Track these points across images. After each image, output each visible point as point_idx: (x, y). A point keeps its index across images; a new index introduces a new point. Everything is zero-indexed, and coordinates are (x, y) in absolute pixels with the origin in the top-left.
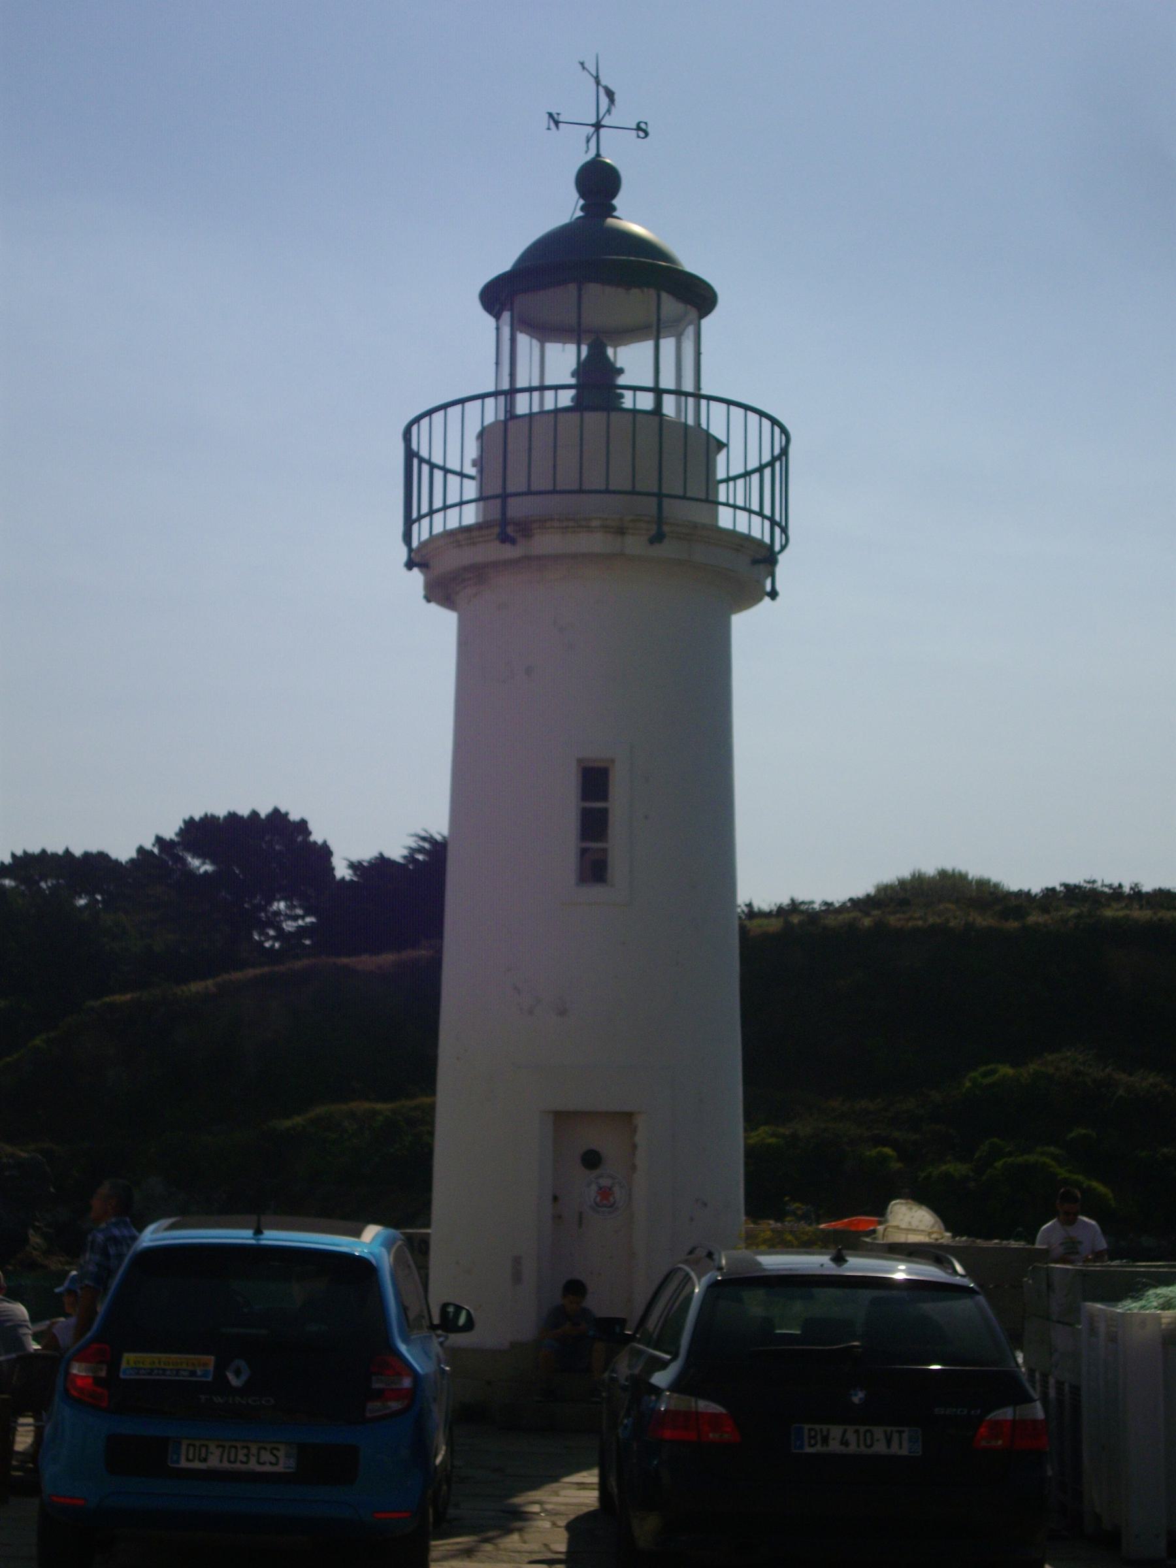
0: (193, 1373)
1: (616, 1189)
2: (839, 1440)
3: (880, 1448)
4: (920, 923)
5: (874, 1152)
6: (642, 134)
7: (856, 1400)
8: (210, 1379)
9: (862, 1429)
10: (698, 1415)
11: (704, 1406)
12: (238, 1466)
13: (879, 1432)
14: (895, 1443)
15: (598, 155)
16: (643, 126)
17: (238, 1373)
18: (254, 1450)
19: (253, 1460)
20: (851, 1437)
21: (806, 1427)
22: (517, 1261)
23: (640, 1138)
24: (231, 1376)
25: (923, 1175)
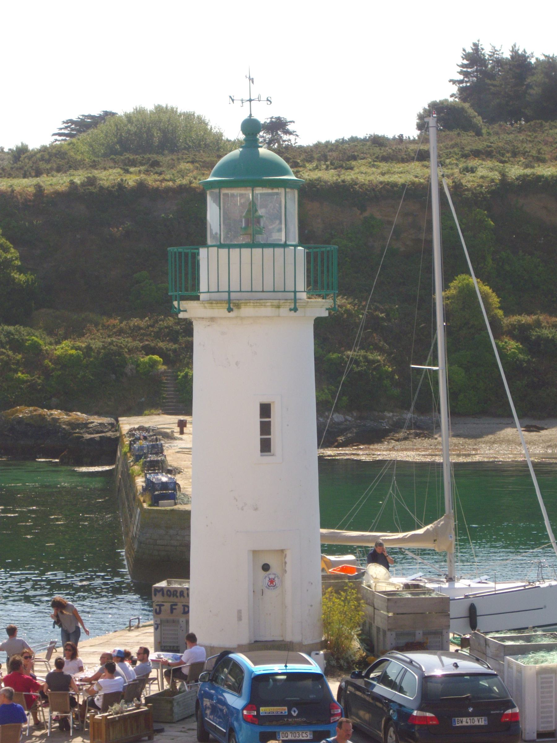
0: (282, 713)
1: (276, 579)
2: (466, 722)
3: (476, 723)
4: (170, 184)
5: (147, 359)
6: (269, 103)
7: (470, 711)
8: (287, 714)
9: (471, 718)
10: (426, 717)
11: (428, 714)
12: (297, 738)
13: (476, 719)
14: (481, 721)
15: (251, 115)
16: (269, 99)
17: (295, 712)
18: (300, 733)
19: (301, 736)
20: (468, 721)
21: (456, 719)
22: (239, 612)
23: (288, 559)
24: (293, 713)
25: (182, 374)
